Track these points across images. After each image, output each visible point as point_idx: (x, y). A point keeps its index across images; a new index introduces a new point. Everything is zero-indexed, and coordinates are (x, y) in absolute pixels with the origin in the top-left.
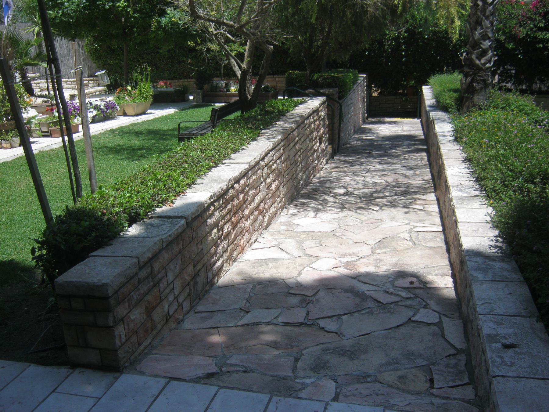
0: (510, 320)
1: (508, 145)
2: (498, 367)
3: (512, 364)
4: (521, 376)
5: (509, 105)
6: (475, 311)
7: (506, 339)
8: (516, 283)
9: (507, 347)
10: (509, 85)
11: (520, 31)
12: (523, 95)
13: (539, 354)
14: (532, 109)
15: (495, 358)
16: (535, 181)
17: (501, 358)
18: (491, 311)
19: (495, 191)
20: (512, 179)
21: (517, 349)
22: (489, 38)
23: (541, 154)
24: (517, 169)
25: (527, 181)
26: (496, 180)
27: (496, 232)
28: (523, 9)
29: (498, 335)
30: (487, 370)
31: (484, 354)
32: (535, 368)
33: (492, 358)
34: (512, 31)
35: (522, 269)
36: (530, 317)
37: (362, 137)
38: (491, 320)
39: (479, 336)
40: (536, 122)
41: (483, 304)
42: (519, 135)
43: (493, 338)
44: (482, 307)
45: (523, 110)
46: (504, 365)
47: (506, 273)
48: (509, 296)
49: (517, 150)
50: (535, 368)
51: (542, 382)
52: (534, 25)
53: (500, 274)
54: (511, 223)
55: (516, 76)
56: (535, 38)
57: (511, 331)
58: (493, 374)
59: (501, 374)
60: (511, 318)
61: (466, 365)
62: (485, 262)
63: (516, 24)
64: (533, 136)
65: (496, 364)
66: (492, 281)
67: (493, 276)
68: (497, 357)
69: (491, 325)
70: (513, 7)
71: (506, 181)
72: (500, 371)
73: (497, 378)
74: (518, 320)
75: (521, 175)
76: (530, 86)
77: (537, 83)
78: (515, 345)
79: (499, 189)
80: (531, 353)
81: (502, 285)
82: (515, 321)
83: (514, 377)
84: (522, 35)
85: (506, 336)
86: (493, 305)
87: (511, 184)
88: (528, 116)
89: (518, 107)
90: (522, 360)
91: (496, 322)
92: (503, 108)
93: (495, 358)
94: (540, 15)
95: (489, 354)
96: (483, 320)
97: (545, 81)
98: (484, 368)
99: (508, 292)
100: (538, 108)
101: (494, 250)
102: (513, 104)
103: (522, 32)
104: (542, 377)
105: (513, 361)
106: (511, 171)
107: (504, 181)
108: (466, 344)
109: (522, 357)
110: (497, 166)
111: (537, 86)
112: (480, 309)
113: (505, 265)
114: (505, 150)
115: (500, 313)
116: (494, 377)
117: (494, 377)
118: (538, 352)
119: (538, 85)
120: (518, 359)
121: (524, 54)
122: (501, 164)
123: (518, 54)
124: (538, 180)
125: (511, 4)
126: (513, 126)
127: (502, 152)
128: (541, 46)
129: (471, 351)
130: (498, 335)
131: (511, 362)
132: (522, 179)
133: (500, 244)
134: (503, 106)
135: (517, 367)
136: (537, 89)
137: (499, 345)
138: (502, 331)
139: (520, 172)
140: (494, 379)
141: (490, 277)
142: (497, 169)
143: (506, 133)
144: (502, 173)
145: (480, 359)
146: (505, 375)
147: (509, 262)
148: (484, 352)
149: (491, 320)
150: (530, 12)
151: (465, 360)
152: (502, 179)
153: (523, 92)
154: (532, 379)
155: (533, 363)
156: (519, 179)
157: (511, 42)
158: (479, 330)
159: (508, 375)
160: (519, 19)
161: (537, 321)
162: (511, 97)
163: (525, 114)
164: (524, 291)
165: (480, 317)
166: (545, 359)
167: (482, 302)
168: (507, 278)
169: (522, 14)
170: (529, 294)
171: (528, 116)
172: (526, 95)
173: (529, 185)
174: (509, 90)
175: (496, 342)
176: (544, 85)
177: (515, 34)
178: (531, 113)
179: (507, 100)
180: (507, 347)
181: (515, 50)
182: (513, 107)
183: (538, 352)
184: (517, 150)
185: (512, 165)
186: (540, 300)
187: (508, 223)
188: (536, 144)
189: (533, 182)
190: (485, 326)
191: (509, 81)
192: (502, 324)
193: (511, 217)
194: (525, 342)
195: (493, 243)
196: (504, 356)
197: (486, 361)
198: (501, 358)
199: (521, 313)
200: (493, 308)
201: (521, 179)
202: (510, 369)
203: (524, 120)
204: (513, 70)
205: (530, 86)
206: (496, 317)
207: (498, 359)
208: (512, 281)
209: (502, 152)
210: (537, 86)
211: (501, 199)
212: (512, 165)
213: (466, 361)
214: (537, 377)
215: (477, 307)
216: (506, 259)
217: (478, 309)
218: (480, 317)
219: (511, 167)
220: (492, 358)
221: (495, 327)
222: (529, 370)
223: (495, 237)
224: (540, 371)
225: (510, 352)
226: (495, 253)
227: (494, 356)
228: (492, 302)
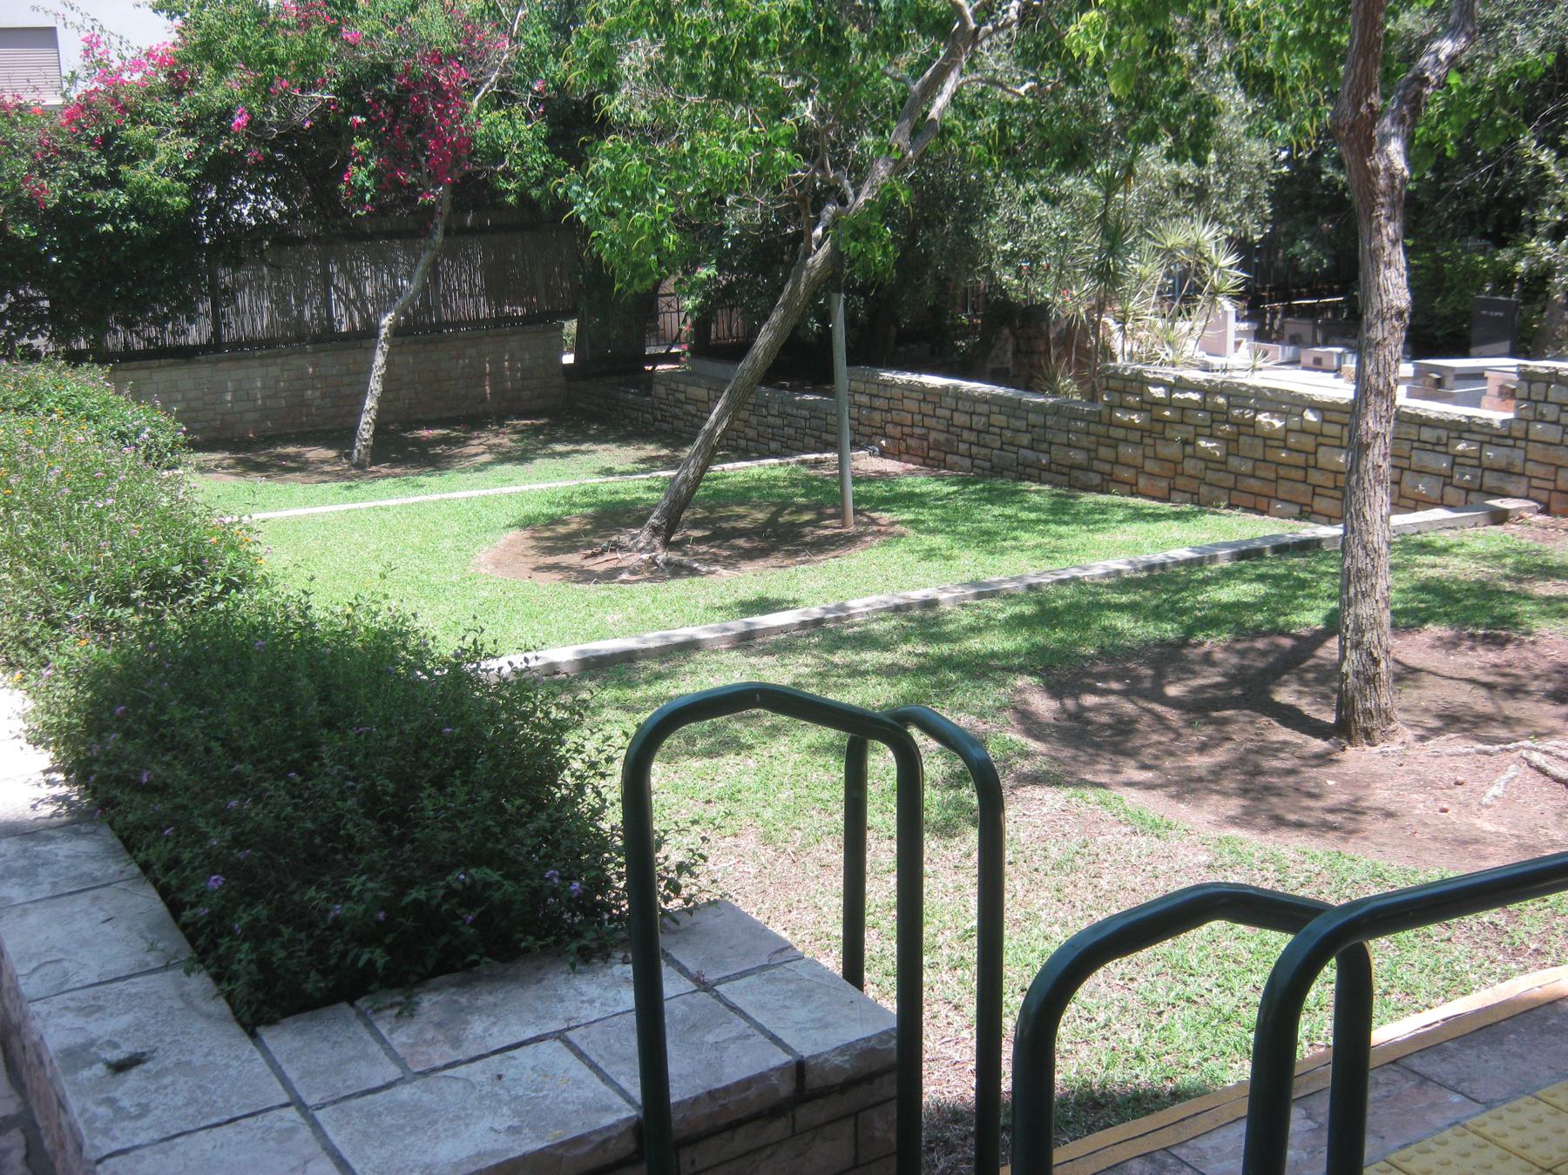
0: (121, 992)
1: (44, 509)
2: (106, 1132)
3: (144, 1110)
4: (174, 1132)
5: (38, 398)
6: (19, 996)
7: (116, 1046)
8: (120, 885)
9: (120, 1067)
10: (40, 342)
11: (42, 189)
12: (75, 366)
13: (211, 1058)
14: (106, 403)
15: (93, 1108)
16: (134, 596)
17: (111, 1102)
18: (62, 984)
19: (25, 643)
20: (67, 603)
21: (149, 1065)
22: (607, 156)
23: (137, 522)
24: (77, 572)
25: (109, 601)
26: (24, 614)
27: (44, 758)
28: (41, 126)
29: (92, 1043)
30: (80, 1148)
31: (65, 1110)
32: (206, 1098)
33: (84, 1111)
34: (20, 190)
35: (129, 842)
36: (167, 967)
37: (712, 431)
38: (67, 1008)
39: (42, 1063)
40: (122, 436)
41: (35, 970)
42: (70, 477)
43: (77, 1056)
44: (36, 977)
45: (81, 407)
46: (123, 1119)
47: (91, 867)
48: (107, 928)
49: (70, 518)
50: (206, 1098)
51: (228, 1130)
52: (81, 171)
53: (74, 873)
54: (77, 725)
55: (54, 316)
56: (90, 206)
57: (125, 1020)
58: (94, 1156)
59: (116, 1146)
60: (121, 985)
61: (27, 1157)
62: (25, 851)
63: (30, 169)
64: (110, 476)
65: (98, 1124)
66: (52, 897)
67: (54, 884)
68: (99, 1103)
69: (69, 1020)
70: (14, 124)
71: (51, 611)
72: (114, 1139)
73: (107, 1162)
74: (140, 985)
75: (92, 588)
76: (98, 341)
77: (116, 332)
78: (143, 1054)
79: (37, 636)
80: (189, 1062)
81: (82, 902)
82: (133, 991)
83: (154, 1143)
84: (52, 200)
85: (116, 1039)
86: (66, 964)
87: (68, 617)
88: (96, 422)
89: (64, 401)
90: (170, 1090)
91: (80, 1010)
92: (20, 409)
93: (93, 1108)
94: (91, 142)
95: (74, 1104)
96: (43, 1015)
97: (137, 324)
98: (70, 1148)
99: (102, 916)
100: (122, 398)
101: (47, 810)
102: (48, 393)
103: (51, 193)
104: (228, 1117)
105: (143, 1101)
106: (63, 580)
107: (47, 612)
108: (18, 1100)
109: (167, 1080)
110: (20, 572)
111: (115, 340)
112: (29, 987)
113: (83, 846)
114: (36, 524)
115: (89, 982)
116: (99, 1161)
117: (99, 1161)
118: (207, 1055)
119: (121, 335)
120: (156, 1090)
121: (64, 251)
122: (30, 564)
123: (48, 255)
124: (139, 592)
125: (7, 115)
126: (49, 455)
127: (28, 529)
128: (110, 228)
129: (36, 1113)
130: (92, 1043)
131: (139, 1105)
132: (96, 598)
133: (61, 790)
134: (22, 401)
135: (157, 1112)
136: (120, 347)
137: (99, 1069)
138: (100, 1028)
139: (87, 580)
140: (99, 1168)
141: (45, 889)
142: (22, 582)
143: (33, 474)
144: (39, 591)
145: (60, 1126)
146: (127, 1145)
147: (94, 832)
148: (62, 1105)
149: (67, 1008)
150: (63, 134)
151: (23, 1143)
152: (39, 606)
153: (75, 358)
154: (203, 1133)
155: (200, 1087)
156: (87, 600)
157: (24, 221)
158: (39, 1045)
159: (137, 1142)
160: (34, 157)
161: (188, 973)
162: (39, 373)
163: (88, 418)
164: (148, 901)
165: (35, 1008)
166: (227, 1066)
167: (34, 964)
168: (95, 879)
169: (41, 142)
170: (160, 907)
171: (96, 422)
172: (85, 365)
173: (118, 612)
174: (33, 356)
175: (90, 1064)
176: (137, 333)
177: (30, 198)
178: (105, 414)
179: (30, 383)
180: (120, 1067)
181: (38, 241)
182: (49, 402)
183: (207, 1055)
184: (70, 518)
185: (62, 563)
186: (187, 915)
187: (70, 727)
188: (120, 495)
189: (127, 602)
190: (51, 1030)
191: (38, 331)
192: (100, 1009)
193: (75, 708)
194: (168, 1039)
195: (46, 792)
196: (118, 1094)
197: (71, 1126)
198: (111, 1102)
199: (147, 964)
200: (66, 973)
201: (92, 598)
202: (139, 1124)
203: (82, 435)
204: (43, 299)
205: (98, 341)
206: (79, 994)
207: (102, 1110)
208: (109, 884)
209: (28, 529)
210: (115, 340)
211: (45, 663)
212: (62, 563)
213: (27, 1146)
214: (215, 1120)
215: (21, 981)
216: (83, 829)
217: (23, 989)
218: (35, 1008)
219: (61, 569)
220: (84, 1111)
221: (80, 1022)
222: (191, 1110)
223: (46, 772)
224: (220, 1104)
225: (133, 1077)
226: (52, 816)
227: (89, 1104)
228: (61, 956)
